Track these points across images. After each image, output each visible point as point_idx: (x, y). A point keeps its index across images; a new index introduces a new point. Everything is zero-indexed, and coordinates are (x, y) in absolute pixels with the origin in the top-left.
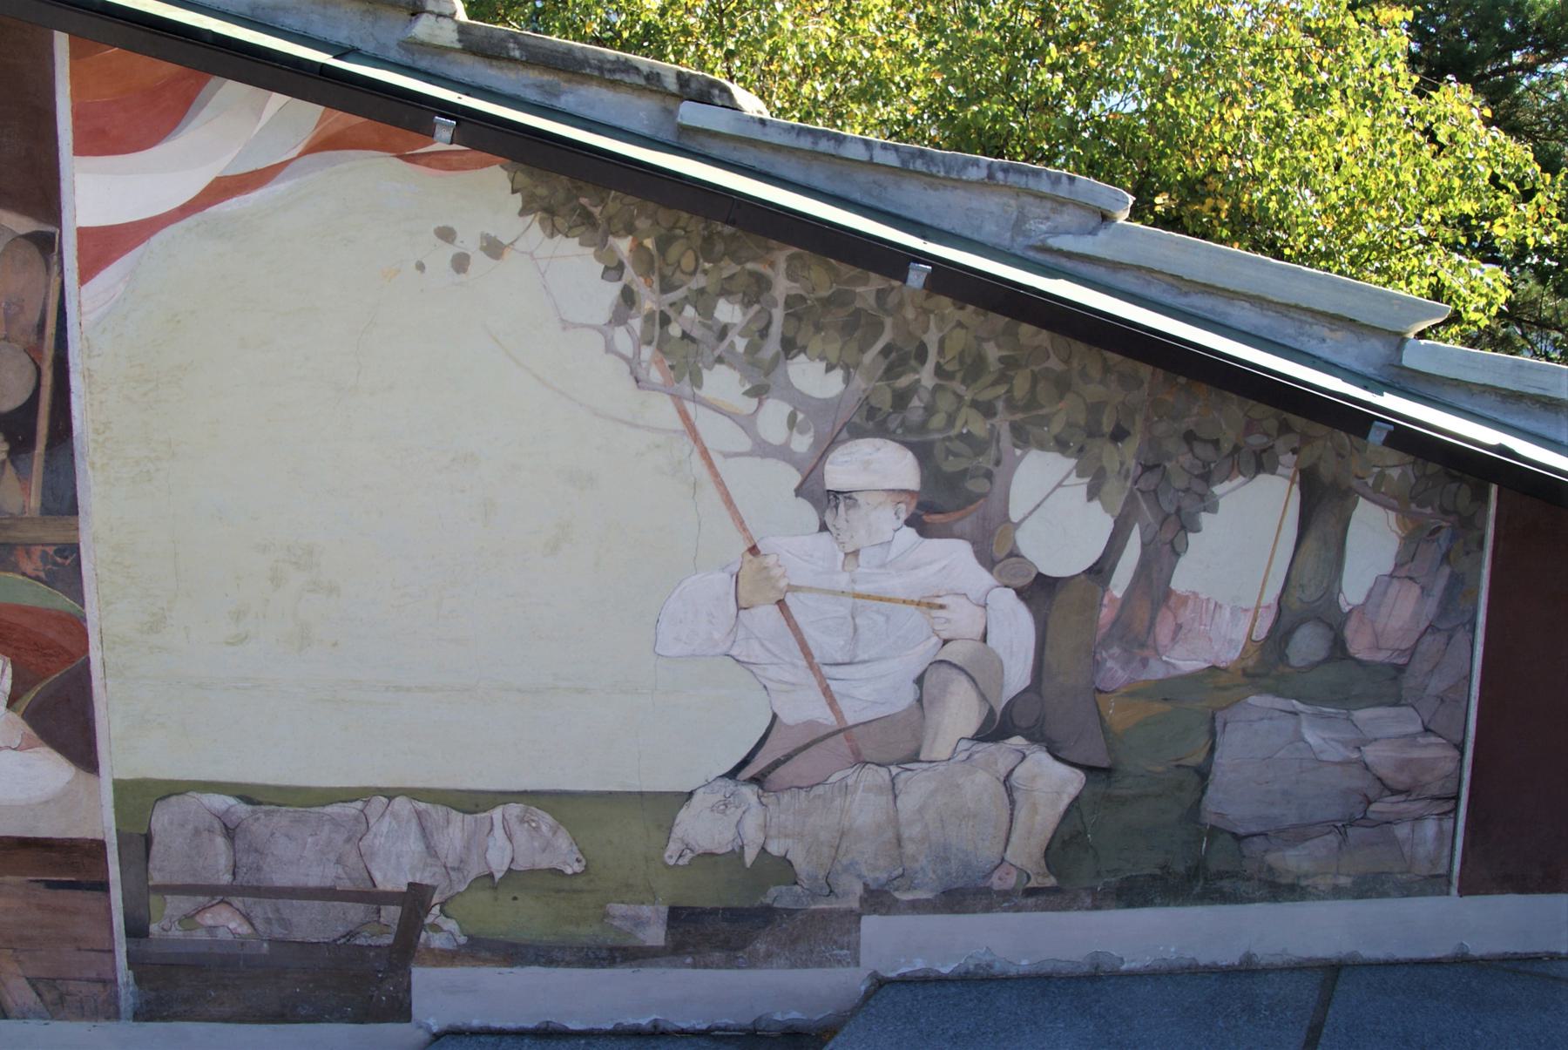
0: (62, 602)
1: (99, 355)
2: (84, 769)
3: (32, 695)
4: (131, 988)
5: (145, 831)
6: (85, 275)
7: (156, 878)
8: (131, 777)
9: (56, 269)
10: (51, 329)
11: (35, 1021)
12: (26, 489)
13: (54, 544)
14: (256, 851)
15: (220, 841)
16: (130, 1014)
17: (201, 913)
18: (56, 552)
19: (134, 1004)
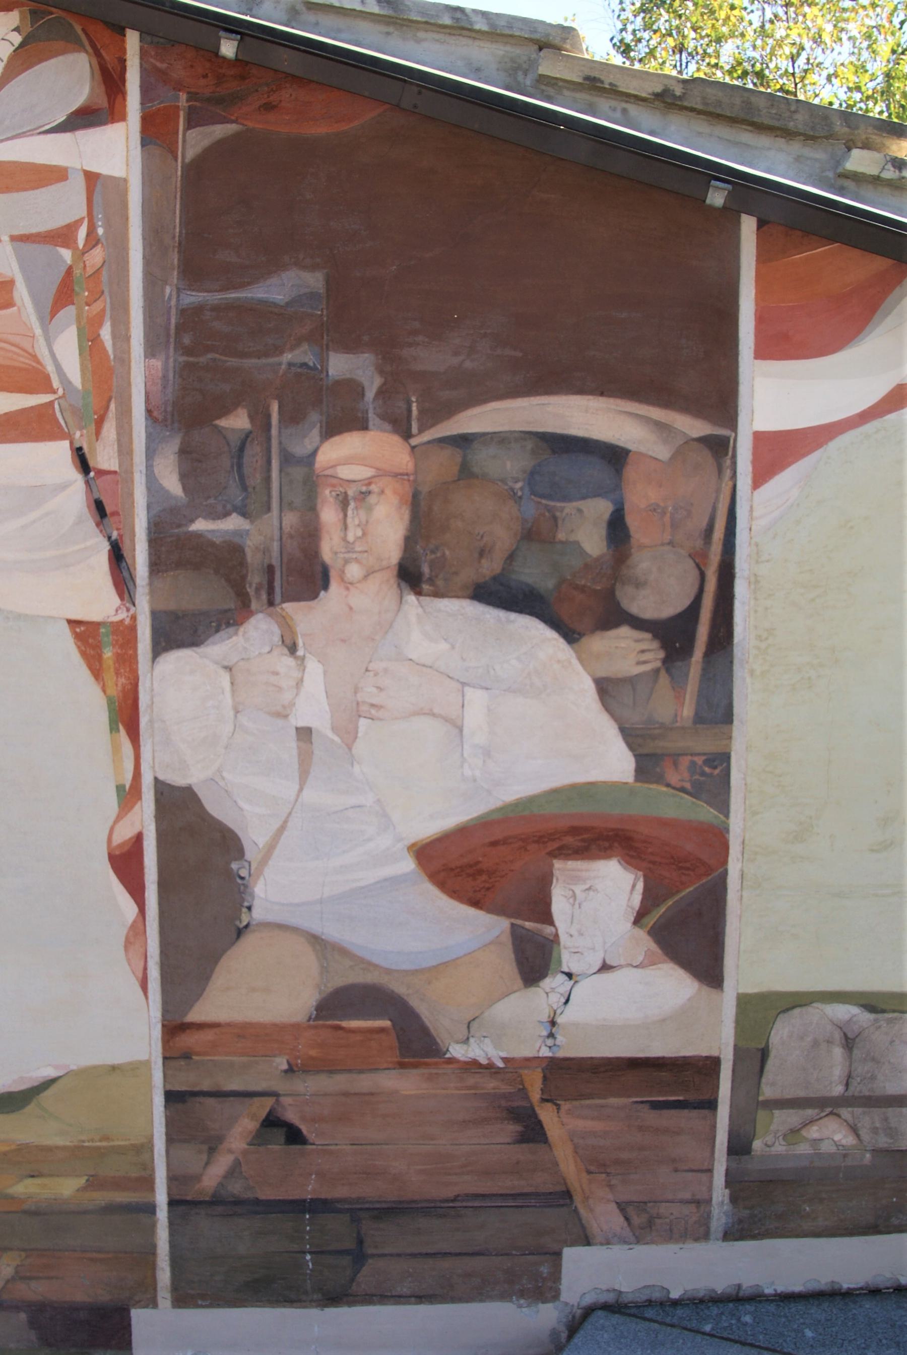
0: (705, 813)
1: (768, 561)
2: (707, 985)
3: (662, 909)
4: (725, 1207)
5: (763, 1046)
6: (759, 480)
7: (768, 1092)
8: (755, 990)
9: (728, 473)
10: (719, 534)
11: (618, 1247)
12: (679, 697)
13: (705, 754)
14: (873, 1059)
15: (838, 1052)
16: (721, 1235)
17: (808, 1127)
18: (707, 762)
19: (726, 1224)
